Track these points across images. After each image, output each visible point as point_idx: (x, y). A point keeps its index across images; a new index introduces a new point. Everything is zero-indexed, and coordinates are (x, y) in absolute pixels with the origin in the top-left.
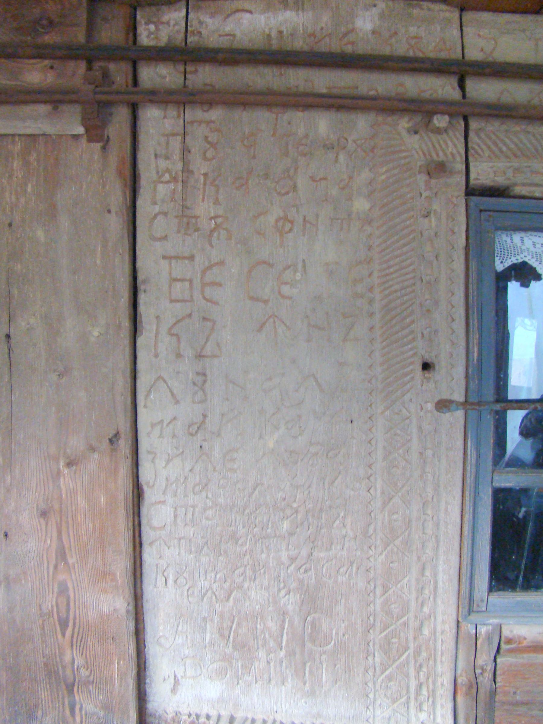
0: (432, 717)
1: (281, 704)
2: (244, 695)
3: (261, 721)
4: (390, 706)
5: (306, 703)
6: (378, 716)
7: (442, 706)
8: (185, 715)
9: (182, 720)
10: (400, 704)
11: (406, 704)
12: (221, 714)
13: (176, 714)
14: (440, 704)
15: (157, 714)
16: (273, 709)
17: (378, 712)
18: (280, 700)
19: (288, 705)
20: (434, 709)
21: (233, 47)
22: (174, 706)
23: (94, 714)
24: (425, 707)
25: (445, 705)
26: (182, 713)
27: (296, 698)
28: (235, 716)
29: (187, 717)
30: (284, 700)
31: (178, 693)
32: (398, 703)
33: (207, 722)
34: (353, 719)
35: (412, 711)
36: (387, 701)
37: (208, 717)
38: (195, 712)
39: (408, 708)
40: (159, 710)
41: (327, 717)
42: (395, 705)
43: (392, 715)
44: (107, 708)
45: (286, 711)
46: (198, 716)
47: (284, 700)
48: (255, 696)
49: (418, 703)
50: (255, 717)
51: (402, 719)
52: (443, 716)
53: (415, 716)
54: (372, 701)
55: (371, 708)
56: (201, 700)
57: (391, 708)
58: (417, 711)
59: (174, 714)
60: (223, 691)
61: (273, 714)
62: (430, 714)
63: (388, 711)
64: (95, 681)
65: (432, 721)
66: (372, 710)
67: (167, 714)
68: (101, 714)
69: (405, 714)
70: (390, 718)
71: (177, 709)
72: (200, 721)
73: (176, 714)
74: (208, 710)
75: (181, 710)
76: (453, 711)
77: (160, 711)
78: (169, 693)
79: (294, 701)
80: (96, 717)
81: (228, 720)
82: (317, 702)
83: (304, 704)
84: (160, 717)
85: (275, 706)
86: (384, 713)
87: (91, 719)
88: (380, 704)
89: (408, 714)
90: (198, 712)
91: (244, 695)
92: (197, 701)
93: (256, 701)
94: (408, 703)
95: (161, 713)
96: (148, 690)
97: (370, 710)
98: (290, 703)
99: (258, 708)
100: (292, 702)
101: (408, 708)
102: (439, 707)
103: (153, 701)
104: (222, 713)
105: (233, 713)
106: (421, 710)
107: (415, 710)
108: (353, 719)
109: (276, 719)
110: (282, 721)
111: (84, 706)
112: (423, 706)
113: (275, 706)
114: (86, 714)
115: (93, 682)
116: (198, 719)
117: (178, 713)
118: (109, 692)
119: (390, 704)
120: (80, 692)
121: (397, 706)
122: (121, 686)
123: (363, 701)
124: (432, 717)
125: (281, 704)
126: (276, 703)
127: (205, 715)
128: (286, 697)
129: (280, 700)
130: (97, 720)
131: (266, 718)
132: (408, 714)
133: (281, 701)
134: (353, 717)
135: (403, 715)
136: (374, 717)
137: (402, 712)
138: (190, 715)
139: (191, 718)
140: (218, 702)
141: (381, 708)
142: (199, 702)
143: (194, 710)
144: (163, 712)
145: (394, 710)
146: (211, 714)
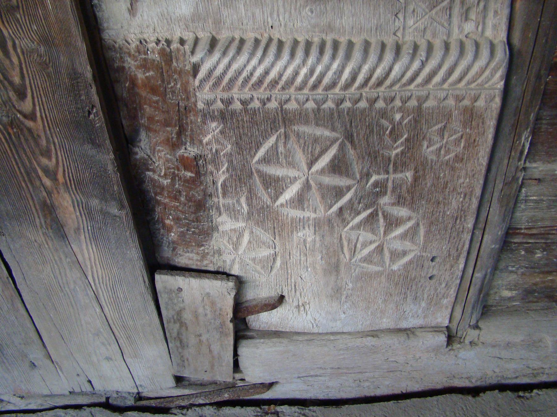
0: (480, 28)
1: (278, 15)
2: (227, 7)
3: (253, 40)
4: (426, 14)
5: (312, 12)
6: (410, 28)
7: (496, 12)
8: (152, 42)
9: (149, 49)
10: (440, 9)
11: (448, 10)
12: (199, 37)
13: (141, 42)
14: (492, 11)
15: (117, 46)
16: (268, 22)
17: (410, 22)
18: (276, 8)
19: (287, 15)
20: (484, 18)
21: (408, 391)
22: (136, 32)
23: (32, 51)
24: (473, 16)
25: (499, 12)
26: (148, 40)
27: (298, 4)
28: (218, 37)
29: (154, 44)
30: (281, 10)
31: (138, 15)
32: (438, 8)
33: (182, 47)
34: (376, 32)
35: (455, 20)
36: (424, 6)
37: (182, 42)
38: (164, 38)
39: (450, 15)
40: (118, 41)
41: (341, 31)
42: (434, 12)
43: (429, 25)
44: (46, 40)
45: (285, 25)
46: (169, 42)
47: (281, 10)
48: (242, 6)
49: (465, 8)
50: (244, 37)
51: (441, 30)
52: (495, 27)
53: (459, 27)
54: (403, 5)
55: (400, 16)
56: (169, 20)
57: (427, 17)
58: (461, 22)
59: (138, 43)
60: (197, 4)
61: (267, 30)
62: (479, 25)
63: (423, 20)
64: (20, 5)
65: (480, 34)
66: (402, 19)
67: (129, 44)
68: (42, 51)
69: (446, 24)
70: (425, 29)
71: (140, 36)
72: (172, 47)
73: (141, 42)
74: (181, 33)
75: (145, 36)
76: (508, 20)
77: (120, 42)
78: (127, 15)
79: (295, 10)
80: (36, 55)
81: (209, 43)
82: (328, 9)
83: (310, 14)
84: (121, 48)
85: (269, 19)
86: (418, 23)
87: (31, 59)
88: (414, 11)
89: (449, 25)
90: (169, 37)
91: (227, 7)
92: (165, 21)
93: (243, 15)
94: (450, 8)
95: (121, 43)
96: (99, 14)
97: (399, 19)
98: (290, 12)
99: (247, 24)
100: (293, 11)
101: (450, 15)
102: (491, 14)
103: (108, 28)
104: (201, 35)
105: (214, 33)
106: (467, 19)
107: (459, 19)
108: (376, 32)
109: (272, 37)
110: (280, 39)
111: (17, 42)
112: (470, 14)
113: (269, 19)
114: (23, 53)
115: (18, 7)
116: (169, 46)
117: (142, 41)
118: (43, 19)
119: (427, 10)
120: (6, 23)
121: (436, 13)
122: (56, 8)
123: (390, 6)
124: (480, 28)
125: (278, 15)
126: (271, 14)
127: (177, 40)
128: (284, 5)
129: (276, 8)
130: (38, 58)
131: (259, 37)
132: (449, 25)
133: (278, 12)
134: (376, 29)
135: (443, 26)
136: (404, 28)
137: (443, 21)
138: (158, 42)
139: (161, 45)
140: (193, 21)
141: (414, 16)
142: (168, 22)
143: (164, 35)
144: (124, 42)
145: (431, 18)
146: (185, 38)
